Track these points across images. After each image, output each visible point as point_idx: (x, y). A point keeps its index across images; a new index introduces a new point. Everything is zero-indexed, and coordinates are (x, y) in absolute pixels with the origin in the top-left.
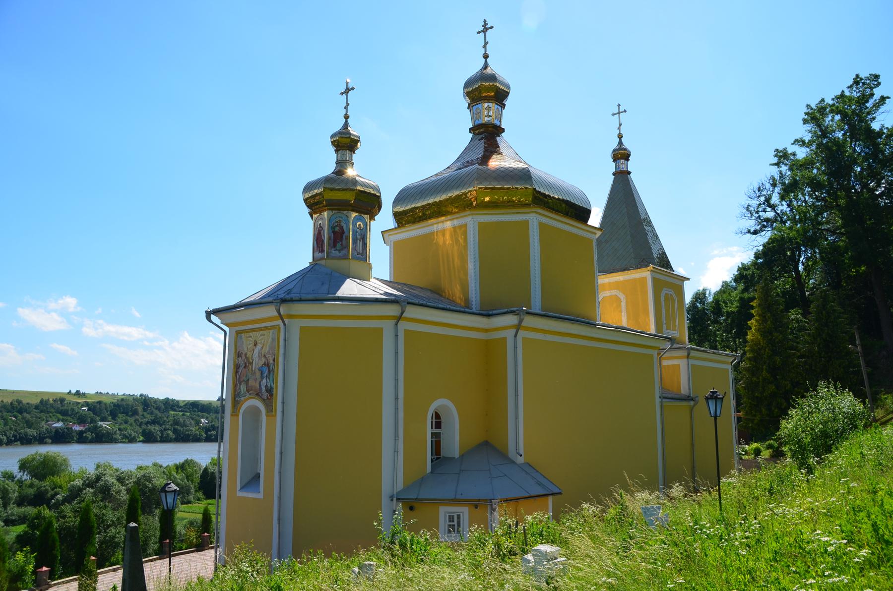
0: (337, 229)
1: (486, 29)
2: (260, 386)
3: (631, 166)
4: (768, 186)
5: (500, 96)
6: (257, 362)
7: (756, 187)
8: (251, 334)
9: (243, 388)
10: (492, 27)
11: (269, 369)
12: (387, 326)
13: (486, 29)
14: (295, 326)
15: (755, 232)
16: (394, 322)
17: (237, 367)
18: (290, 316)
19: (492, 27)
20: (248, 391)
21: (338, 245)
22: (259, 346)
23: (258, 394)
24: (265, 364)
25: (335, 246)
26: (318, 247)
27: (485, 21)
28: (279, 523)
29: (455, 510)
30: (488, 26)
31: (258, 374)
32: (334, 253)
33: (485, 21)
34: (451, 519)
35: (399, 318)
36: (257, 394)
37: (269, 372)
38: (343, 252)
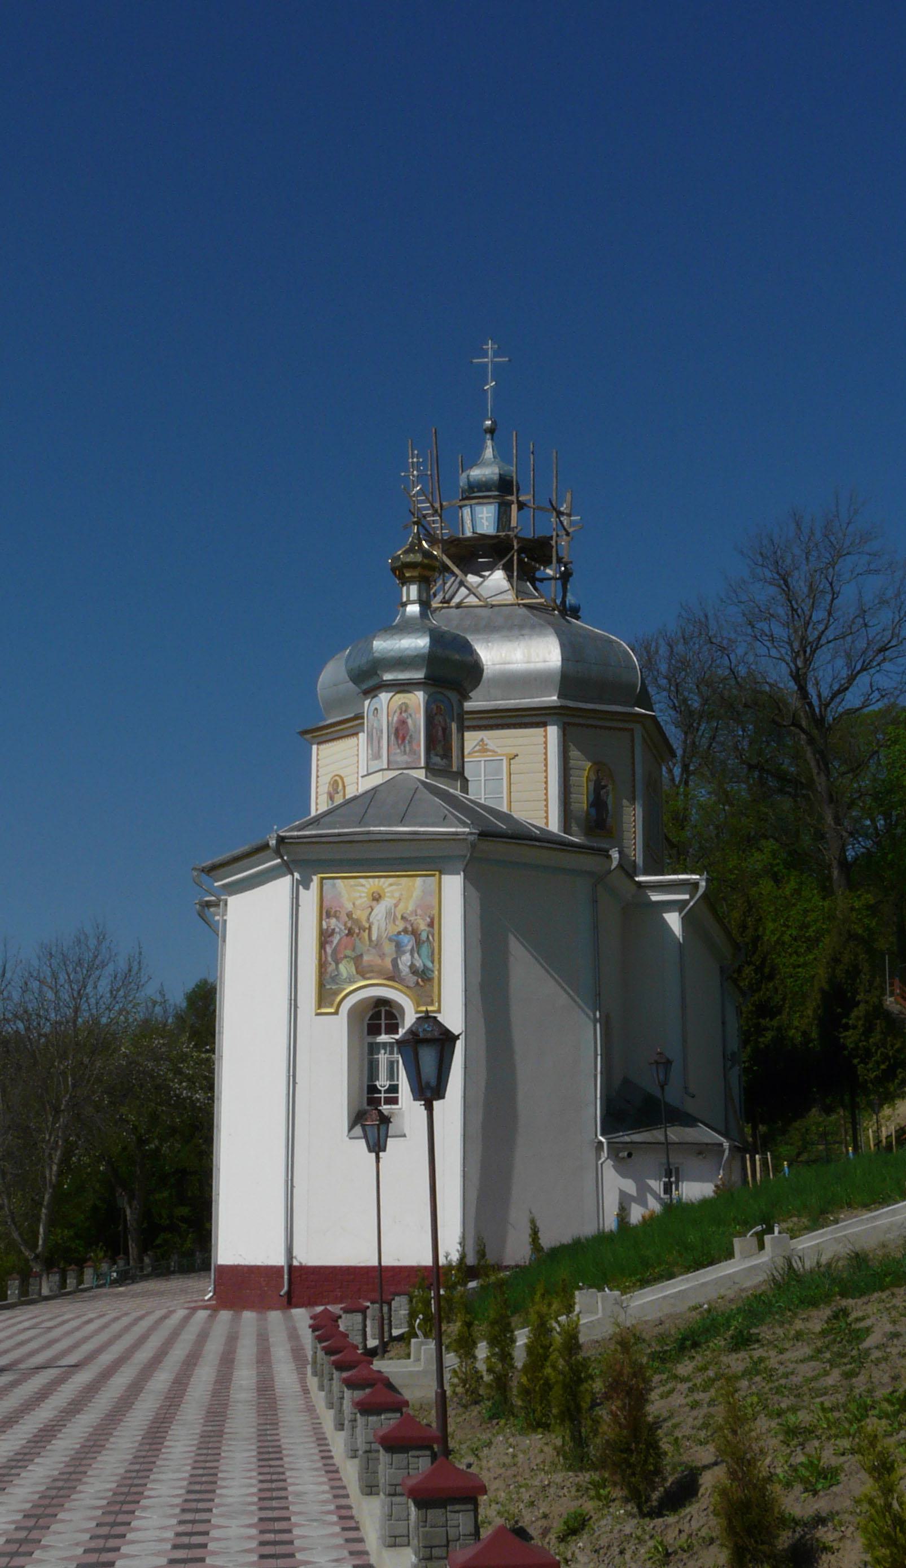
9: (346, 969)
31: (389, 948)
37: (419, 943)
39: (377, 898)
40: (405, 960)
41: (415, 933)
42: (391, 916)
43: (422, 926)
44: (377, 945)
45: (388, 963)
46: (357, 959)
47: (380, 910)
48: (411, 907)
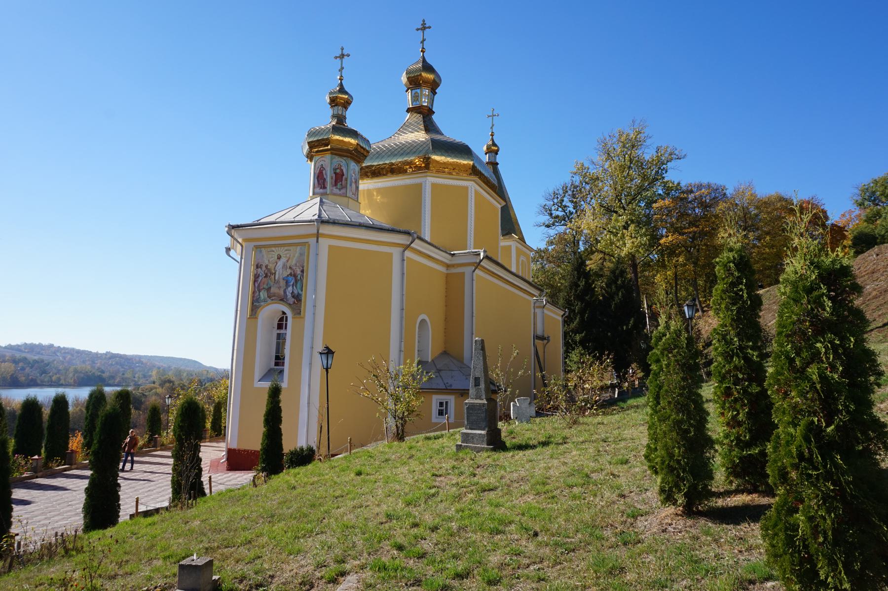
0: (338, 171)
1: (424, 28)
2: (285, 292)
3: (499, 159)
4: (561, 192)
5: (434, 86)
6: (281, 272)
7: (551, 191)
8: (273, 249)
9: (263, 295)
10: (429, 27)
11: (297, 278)
12: (396, 252)
13: (424, 28)
14: (324, 243)
15: (548, 226)
16: (401, 249)
17: (256, 277)
18: (324, 236)
19: (429, 27)
20: (269, 297)
21: (339, 186)
22: (283, 260)
23: (283, 300)
24: (291, 274)
25: (336, 185)
26: (319, 184)
27: (424, 21)
28: (309, 406)
29: (443, 398)
30: (427, 26)
31: (282, 283)
32: (336, 190)
33: (424, 21)
34: (441, 404)
35: (407, 247)
36: (282, 300)
37: (296, 281)
38: (343, 191)
39: (279, 258)
40: (290, 289)
41: (295, 276)
42: (284, 267)
43: (299, 272)
44: (276, 282)
45: (282, 293)
46: (269, 289)
47: (280, 263)
48: (294, 262)
